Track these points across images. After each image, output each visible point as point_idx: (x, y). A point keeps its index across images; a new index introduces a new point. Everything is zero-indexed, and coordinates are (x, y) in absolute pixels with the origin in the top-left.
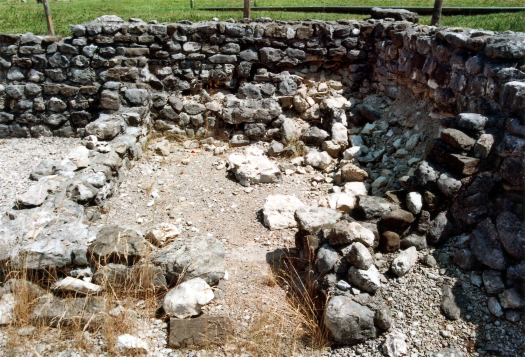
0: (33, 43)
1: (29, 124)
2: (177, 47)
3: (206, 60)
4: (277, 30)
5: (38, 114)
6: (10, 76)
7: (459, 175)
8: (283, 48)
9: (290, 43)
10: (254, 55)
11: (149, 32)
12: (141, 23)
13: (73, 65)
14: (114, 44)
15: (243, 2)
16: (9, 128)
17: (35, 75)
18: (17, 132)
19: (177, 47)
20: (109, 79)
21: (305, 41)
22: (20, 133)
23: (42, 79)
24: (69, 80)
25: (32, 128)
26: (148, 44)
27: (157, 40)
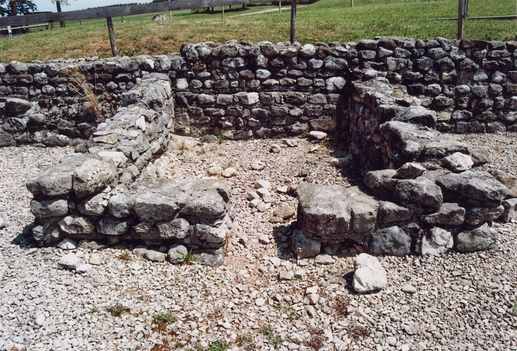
1: (489, 120)
5: (497, 112)
6: (475, 78)
15: (455, 5)
16: (468, 124)
17: (499, 76)
18: (476, 129)
22: (478, 129)
23: (505, 80)
25: (489, 124)
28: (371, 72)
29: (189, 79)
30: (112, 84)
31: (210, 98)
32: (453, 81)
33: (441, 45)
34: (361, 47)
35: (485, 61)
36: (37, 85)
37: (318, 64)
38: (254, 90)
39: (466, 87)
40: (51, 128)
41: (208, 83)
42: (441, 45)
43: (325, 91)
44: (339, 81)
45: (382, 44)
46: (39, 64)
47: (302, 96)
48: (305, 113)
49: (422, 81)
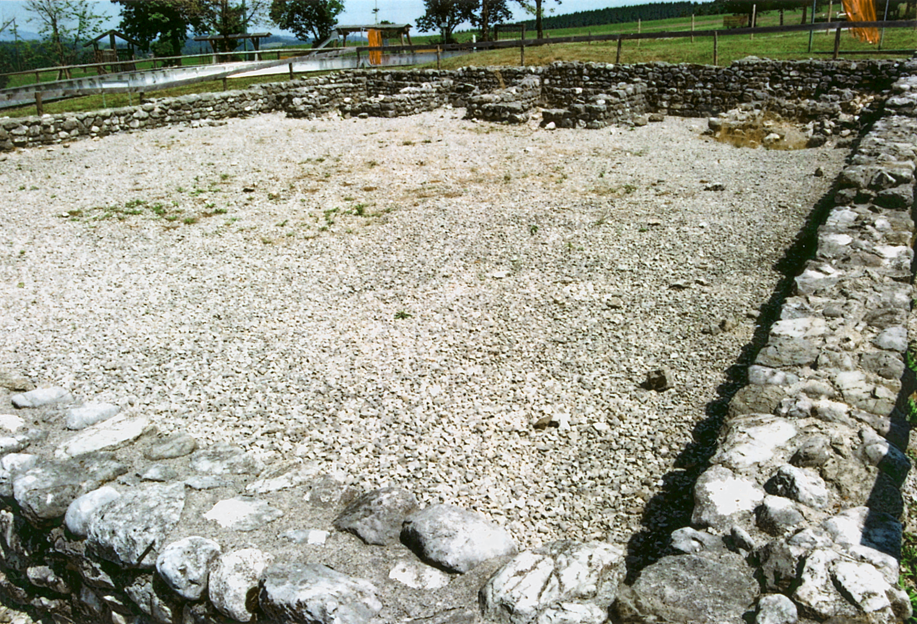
0: (711, 69)
1: (702, 110)
2: (786, 73)
3: (802, 81)
4: (845, 65)
8: (848, 75)
9: (853, 72)
10: (830, 79)
11: (772, 65)
12: (768, 60)
13: (730, 81)
14: (752, 71)
19: (786, 73)
20: (747, 87)
21: (862, 71)
24: (726, 89)
26: (771, 71)
27: (776, 70)
29: (550, 79)
31: (558, 89)
32: (684, 87)
35: (701, 77)
36: (480, 78)
38: (581, 87)
39: (690, 91)
46: (482, 68)
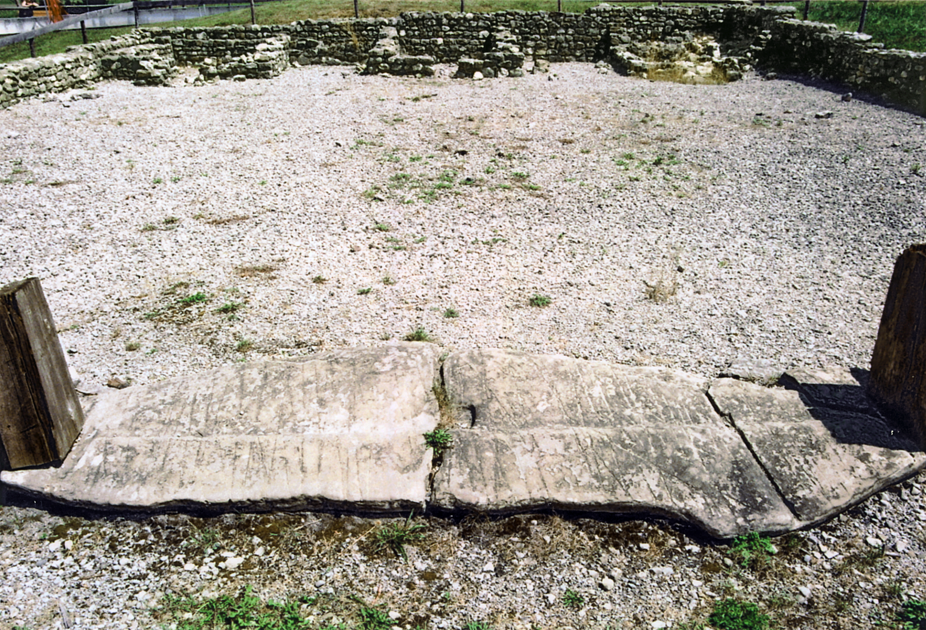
1: (566, 55)
3: (650, 25)
7: (761, 45)
9: (689, 16)
17: (571, 31)
24: (587, 34)
28: (501, 28)
29: (407, 31)
30: (365, 32)
31: (418, 41)
33: (539, 14)
34: (497, 15)
36: (323, 32)
37: (474, 24)
38: (441, 37)
39: (553, 37)
40: (330, 55)
41: (416, 33)
42: (539, 14)
43: (478, 39)
44: (486, 33)
45: (508, 13)
47: (466, 41)
48: (468, 50)
49: (529, 33)
